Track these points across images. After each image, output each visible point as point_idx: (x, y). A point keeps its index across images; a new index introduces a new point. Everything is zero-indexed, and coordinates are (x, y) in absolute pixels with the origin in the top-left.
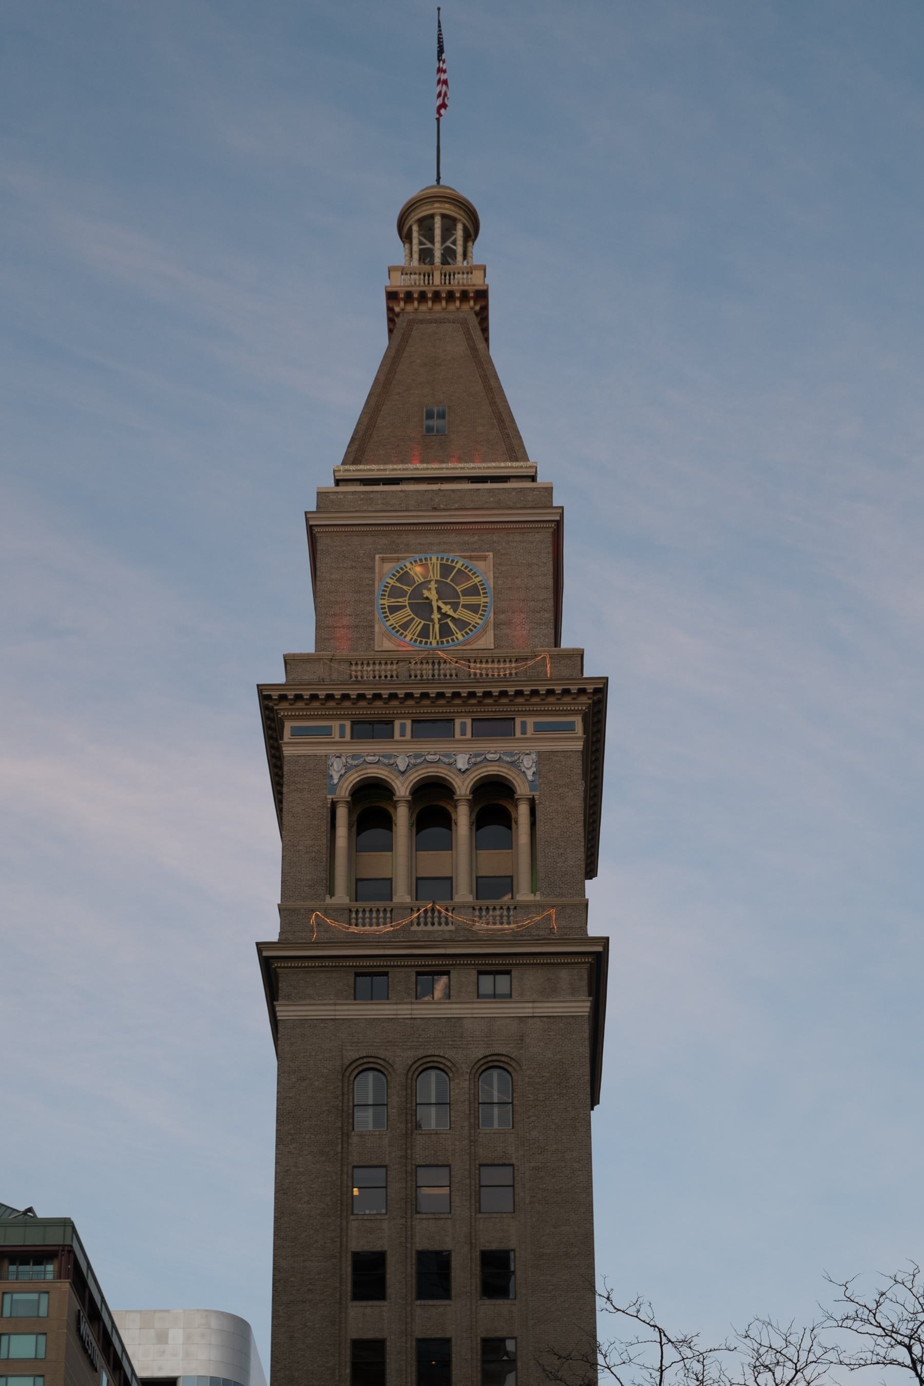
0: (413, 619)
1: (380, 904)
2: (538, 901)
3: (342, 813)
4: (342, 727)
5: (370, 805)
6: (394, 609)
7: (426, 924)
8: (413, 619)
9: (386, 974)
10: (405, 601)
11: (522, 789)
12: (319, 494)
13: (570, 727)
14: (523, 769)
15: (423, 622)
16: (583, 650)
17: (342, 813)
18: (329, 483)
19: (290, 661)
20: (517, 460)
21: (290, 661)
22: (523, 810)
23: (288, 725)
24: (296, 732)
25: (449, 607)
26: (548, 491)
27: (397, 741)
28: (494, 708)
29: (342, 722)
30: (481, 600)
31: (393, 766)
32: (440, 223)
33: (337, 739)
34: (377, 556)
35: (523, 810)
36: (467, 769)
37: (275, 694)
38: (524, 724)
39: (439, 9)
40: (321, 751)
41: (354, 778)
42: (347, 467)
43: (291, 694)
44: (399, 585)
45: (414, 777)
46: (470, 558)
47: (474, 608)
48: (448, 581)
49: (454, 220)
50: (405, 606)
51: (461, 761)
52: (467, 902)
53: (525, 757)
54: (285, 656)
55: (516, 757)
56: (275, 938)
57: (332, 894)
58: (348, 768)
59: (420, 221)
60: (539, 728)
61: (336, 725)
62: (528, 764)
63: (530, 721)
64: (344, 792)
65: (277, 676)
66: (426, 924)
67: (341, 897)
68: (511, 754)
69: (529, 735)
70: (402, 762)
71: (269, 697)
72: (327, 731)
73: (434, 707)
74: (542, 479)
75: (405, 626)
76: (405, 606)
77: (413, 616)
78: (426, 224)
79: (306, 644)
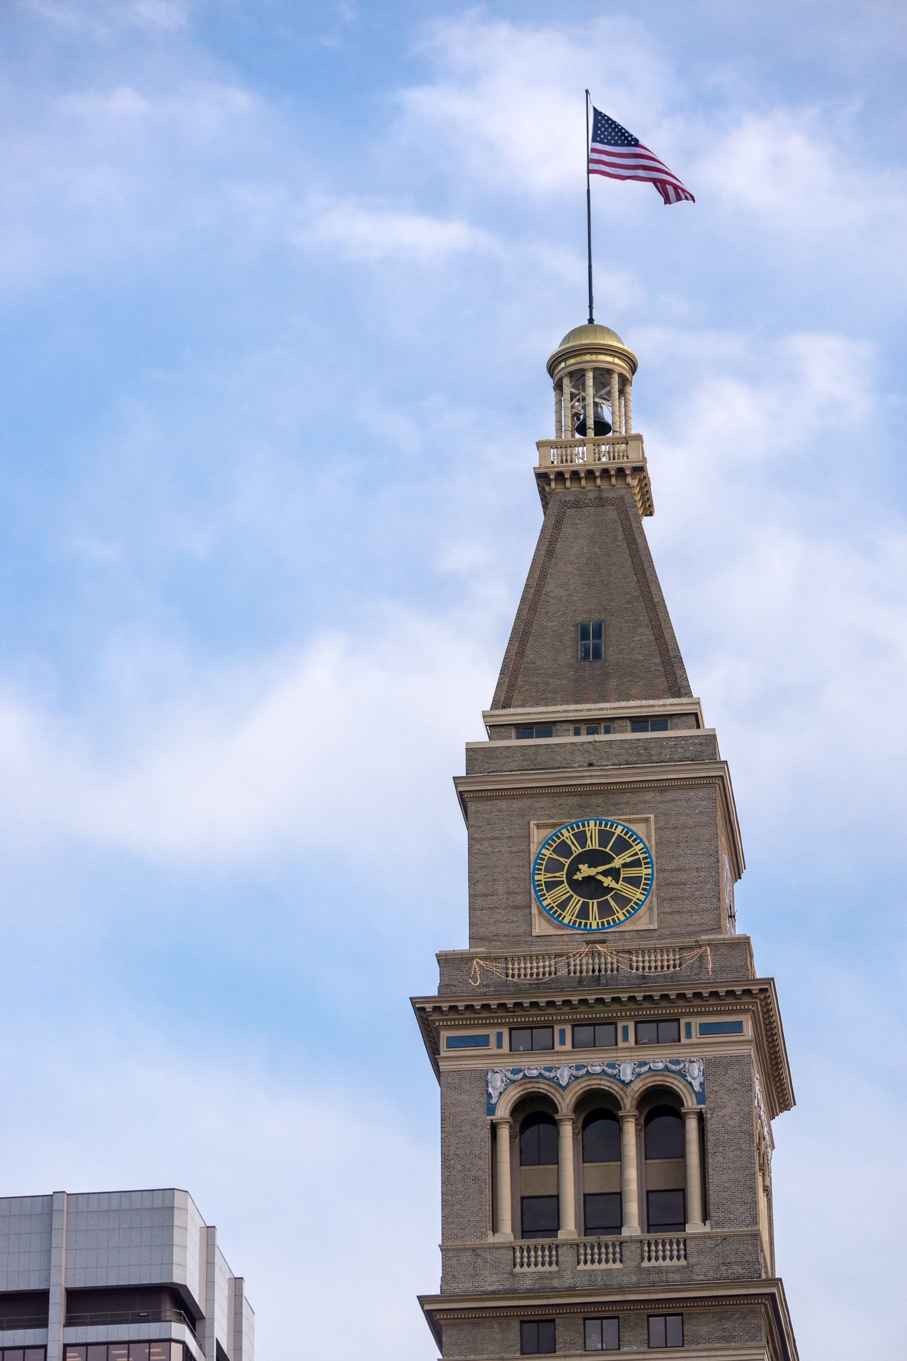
0: (571, 896)
1: (546, 1241)
2: (708, 1233)
3: (504, 1134)
4: (500, 1036)
6: (551, 885)
7: (593, 1262)
8: (571, 896)
9: (553, 1321)
10: (562, 875)
11: (690, 1103)
12: (468, 750)
13: (737, 1027)
14: (689, 1079)
15: (582, 900)
16: (748, 938)
17: (504, 1134)
18: (481, 736)
19: (445, 960)
20: (679, 696)
21: (445, 960)
22: (692, 1125)
23: (444, 1035)
24: (453, 1043)
25: (610, 878)
26: (711, 739)
27: (558, 1052)
28: (660, 1010)
29: (500, 1030)
30: (644, 871)
31: (555, 1081)
32: (588, 372)
33: (495, 1051)
34: (532, 823)
35: (692, 1125)
36: (631, 1081)
37: (429, 1007)
38: (688, 1025)
39: (587, 92)
40: (479, 1064)
42: (496, 712)
43: (445, 1006)
44: (555, 857)
45: (578, 1089)
46: (630, 821)
47: (634, 882)
48: (607, 850)
49: (610, 372)
50: (562, 882)
51: (629, 1067)
52: (636, 1236)
53: (689, 1062)
54: (437, 955)
55: (682, 1066)
56: (437, 1291)
57: (495, 1229)
59: (571, 374)
60: (706, 1029)
61: (492, 1033)
62: (696, 1071)
63: (696, 1022)
64: (503, 1111)
65: (429, 987)
66: (593, 1262)
68: (677, 1062)
69: (694, 1040)
70: (566, 1070)
71: (422, 1009)
72: (483, 1041)
73: (592, 1009)
74: (708, 722)
75: (563, 906)
76: (562, 882)
77: (571, 893)
78: (577, 376)
79: (461, 942)
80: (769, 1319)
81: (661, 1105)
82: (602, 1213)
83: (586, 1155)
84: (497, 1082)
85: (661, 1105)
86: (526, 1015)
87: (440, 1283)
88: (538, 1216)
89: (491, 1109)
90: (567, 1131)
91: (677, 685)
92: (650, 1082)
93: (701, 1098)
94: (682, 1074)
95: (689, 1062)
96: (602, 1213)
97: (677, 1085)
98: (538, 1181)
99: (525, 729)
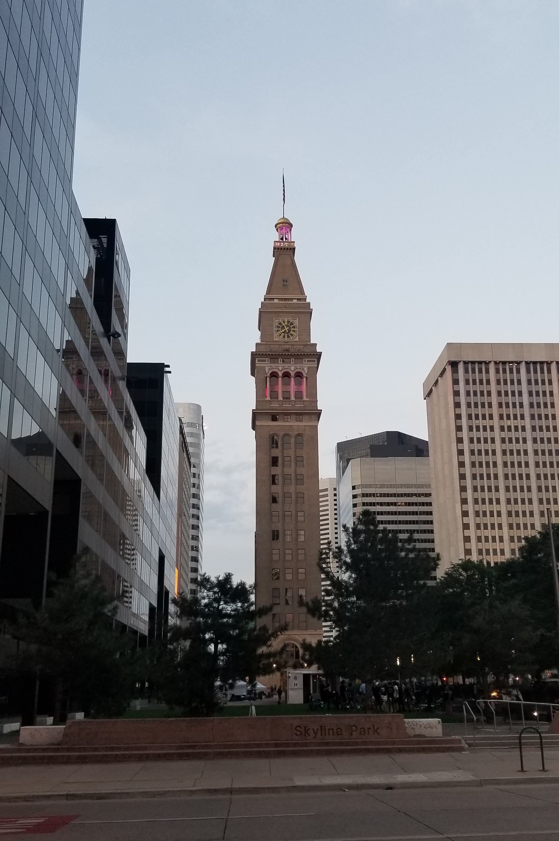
5: (274, 375)
11: (305, 375)
17: (268, 379)
22: (305, 379)
24: (259, 361)
28: (299, 356)
40: (264, 365)
41: (271, 371)
51: (292, 368)
58: (269, 369)
60: (308, 361)
61: (267, 359)
63: (306, 359)
64: (269, 375)
67: (268, 398)
70: (280, 367)
72: (265, 361)
81: (299, 375)
83: (284, 384)
85: (299, 375)
86: (274, 357)
90: (280, 379)
91: (302, 292)
93: (307, 374)
95: (304, 367)
97: (303, 372)
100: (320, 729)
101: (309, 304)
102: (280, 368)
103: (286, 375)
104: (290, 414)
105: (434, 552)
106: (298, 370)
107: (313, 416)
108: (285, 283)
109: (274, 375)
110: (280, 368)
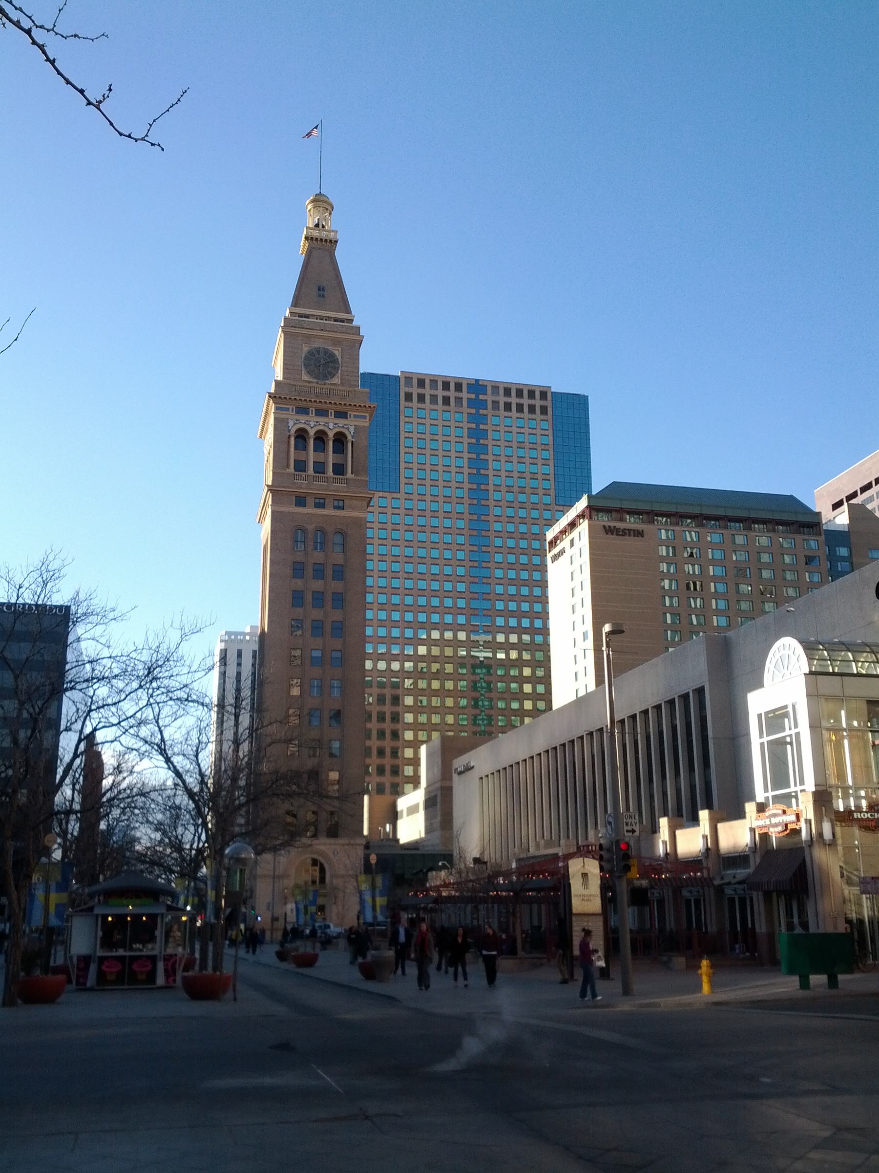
11: (349, 437)
17: (292, 439)
40: (287, 416)
51: (332, 425)
58: (295, 424)
60: (355, 416)
61: (290, 407)
62: (352, 429)
63: (352, 414)
67: (292, 469)
80: (827, 1017)
81: (340, 440)
82: (320, 468)
84: (291, 423)
87: (557, 387)
88: (300, 466)
89: (289, 431)
91: (348, 311)
92: (338, 430)
93: (353, 437)
94: (348, 429)
96: (320, 468)
97: (346, 432)
98: (302, 456)
99: (300, 316)
100: (780, 661)
101: (358, 329)
102: (312, 424)
103: (321, 437)
104: (709, 518)
105: (321, 950)
106: (321, 428)
107: (601, 514)
108: (321, 292)
109: (301, 435)
110: (312, 424)
